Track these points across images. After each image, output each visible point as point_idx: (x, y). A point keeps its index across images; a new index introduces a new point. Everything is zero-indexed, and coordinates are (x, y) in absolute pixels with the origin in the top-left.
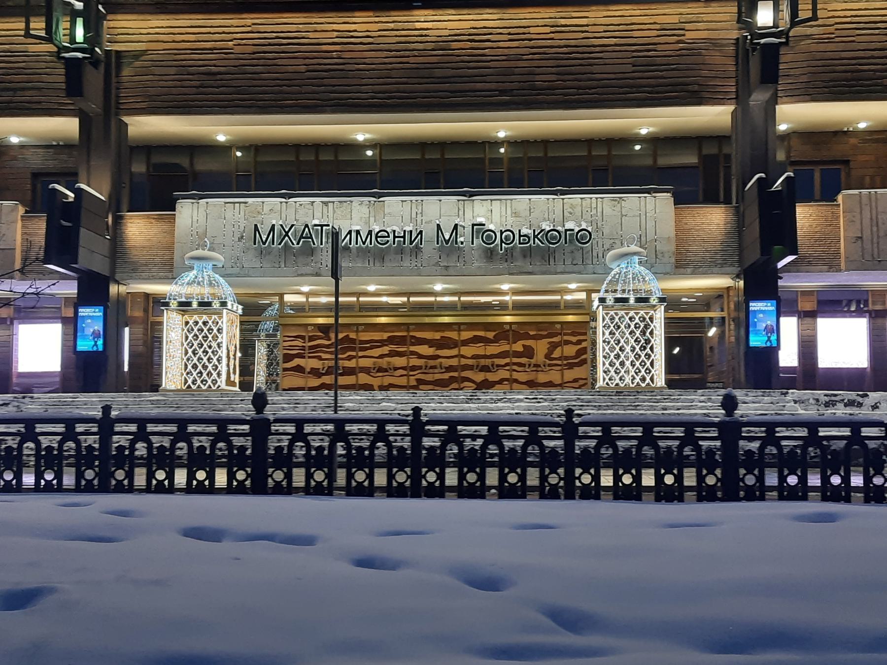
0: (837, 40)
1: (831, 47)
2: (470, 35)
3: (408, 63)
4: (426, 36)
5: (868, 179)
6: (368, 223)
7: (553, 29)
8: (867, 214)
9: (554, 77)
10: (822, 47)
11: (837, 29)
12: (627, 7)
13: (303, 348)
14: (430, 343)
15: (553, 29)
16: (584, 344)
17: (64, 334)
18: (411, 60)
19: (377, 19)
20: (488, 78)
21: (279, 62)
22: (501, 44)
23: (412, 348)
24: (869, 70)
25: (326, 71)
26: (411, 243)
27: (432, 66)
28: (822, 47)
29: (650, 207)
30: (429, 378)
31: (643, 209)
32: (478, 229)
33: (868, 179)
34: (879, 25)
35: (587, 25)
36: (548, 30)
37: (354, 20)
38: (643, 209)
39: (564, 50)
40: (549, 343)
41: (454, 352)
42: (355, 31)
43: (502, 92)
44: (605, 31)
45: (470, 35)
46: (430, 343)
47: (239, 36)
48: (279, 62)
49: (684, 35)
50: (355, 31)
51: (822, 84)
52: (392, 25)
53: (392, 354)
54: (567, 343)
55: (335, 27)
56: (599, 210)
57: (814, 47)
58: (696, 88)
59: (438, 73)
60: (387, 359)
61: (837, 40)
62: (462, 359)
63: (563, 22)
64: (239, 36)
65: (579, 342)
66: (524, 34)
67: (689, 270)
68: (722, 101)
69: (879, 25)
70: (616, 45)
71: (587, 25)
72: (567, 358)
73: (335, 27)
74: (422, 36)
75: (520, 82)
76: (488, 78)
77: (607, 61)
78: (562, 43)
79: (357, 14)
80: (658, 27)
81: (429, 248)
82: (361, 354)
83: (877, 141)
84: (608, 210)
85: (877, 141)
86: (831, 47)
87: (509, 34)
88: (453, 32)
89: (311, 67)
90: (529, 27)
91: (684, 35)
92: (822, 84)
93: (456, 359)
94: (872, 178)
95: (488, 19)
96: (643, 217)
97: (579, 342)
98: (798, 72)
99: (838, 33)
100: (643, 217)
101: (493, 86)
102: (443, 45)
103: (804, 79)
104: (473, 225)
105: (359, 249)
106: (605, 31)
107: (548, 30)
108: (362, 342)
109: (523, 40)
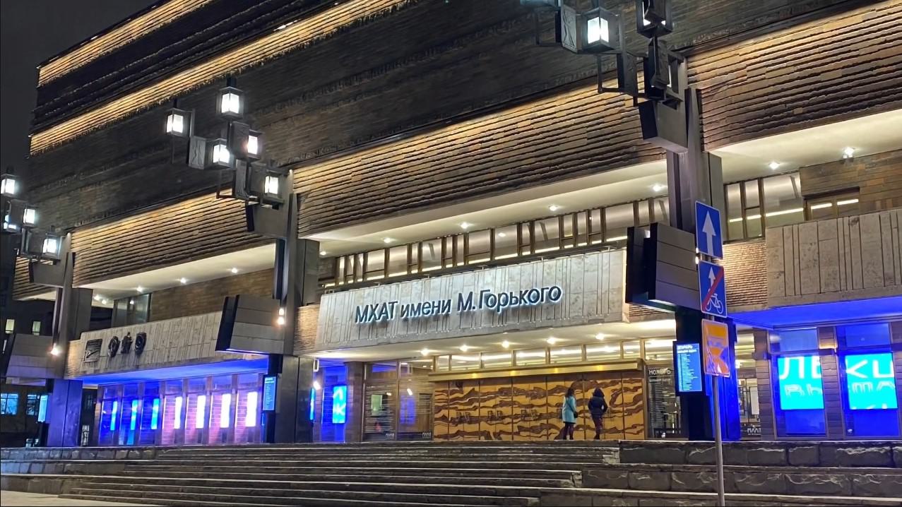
0: (749, 80)
1: (745, 88)
2: (480, 138)
3: (444, 168)
4: (454, 145)
5: (878, 204)
6: (420, 298)
7: (533, 121)
8: (788, 246)
9: (533, 160)
10: (736, 90)
11: (748, 71)
12: (582, 91)
13: (447, 401)
14: (526, 393)
15: (533, 121)
16: (640, 391)
17: (258, 396)
18: (445, 165)
19: (426, 139)
20: (492, 170)
21: (375, 183)
22: (500, 141)
23: (515, 399)
24: (781, 103)
25: (398, 184)
26: (443, 311)
27: (460, 166)
28: (736, 90)
29: (605, 261)
30: (526, 425)
31: (600, 264)
32: (486, 297)
33: (878, 204)
34: (786, 58)
35: (555, 113)
36: (530, 122)
37: (416, 142)
38: (600, 264)
39: (541, 136)
40: (613, 390)
41: (543, 401)
42: (415, 151)
43: (501, 178)
44: (567, 115)
45: (480, 138)
46: (526, 393)
47: (354, 169)
48: (375, 183)
49: (624, 105)
50: (415, 151)
51: (738, 125)
52: (435, 142)
53: (502, 404)
54: (627, 390)
55: (404, 150)
56: (569, 268)
57: (729, 92)
58: (634, 149)
59: (462, 171)
60: (499, 409)
61: (749, 80)
62: (549, 408)
63: (539, 114)
64: (354, 169)
65: (636, 389)
66: (514, 129)
67: (642, 317)
68: (658, 157)
69: (786, 58)
70: (575, 124)
71: (555, 113)
72: (627, 405)
73: (404, 150)
74: (452, 145)
75: (500, 171)
76: (492, 170)
77: (570, 139)
78: (538, 131)
79: (415, 138)
80: (605, 102)
81: (454, 312)
82: (482, 404)
83: (885, 163)
84: (575, 267)
85: (885, 163)
86: (745, 88)
87: (505, 131)
88: (470, 138)
89: (391, 183)
90: (517, 123)
91: (624, 105)
92: (738, 125)
93: (545, 408)
94: (883, 201)
95: (491, 123)
96: (600, 271)
97: (636, 389)
98: (718, 118)
99: (749, 74)
100: (600, 271)
101: (495, 175)
102: (464, 150)
103: (723, 123)
104: (482, 292)
105: (414, 319)
106: (567, 115)
107: (530, 122)
108: (484, 394)
109: (513, 134)
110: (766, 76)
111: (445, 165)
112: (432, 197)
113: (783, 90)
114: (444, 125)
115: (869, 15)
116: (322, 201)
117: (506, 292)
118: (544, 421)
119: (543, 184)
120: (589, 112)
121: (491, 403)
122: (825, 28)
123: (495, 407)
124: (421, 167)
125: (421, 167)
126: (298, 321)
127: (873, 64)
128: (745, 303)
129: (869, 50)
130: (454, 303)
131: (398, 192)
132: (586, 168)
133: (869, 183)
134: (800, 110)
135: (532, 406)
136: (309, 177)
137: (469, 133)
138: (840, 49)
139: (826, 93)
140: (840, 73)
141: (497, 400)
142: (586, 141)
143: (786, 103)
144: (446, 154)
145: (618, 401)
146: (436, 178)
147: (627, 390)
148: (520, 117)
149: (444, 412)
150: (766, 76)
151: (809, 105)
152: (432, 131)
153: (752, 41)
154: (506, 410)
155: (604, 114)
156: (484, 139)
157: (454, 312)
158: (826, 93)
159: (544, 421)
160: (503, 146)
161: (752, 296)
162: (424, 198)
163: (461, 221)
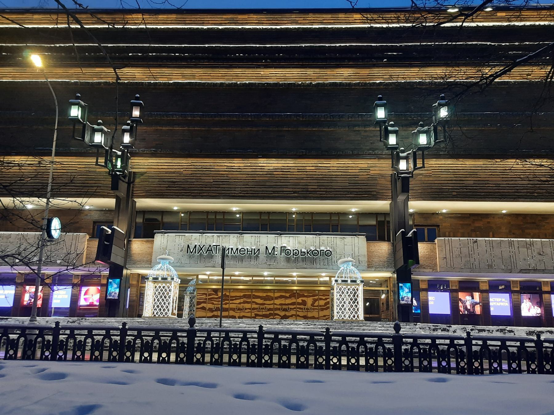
5: (447, 233)
10: (427, 179)
16: (328, 300)
18: (257, 178)
20: (289, 187)
22: (294, 173)
28: (427, 179)
41: (272, 302)
43: (295, 192)
48: (202, 178)
53: (245, 302)
54: (321, 299)
55: (226, 164)
57: (423, 179)
63: (320, 165)
65: (326, 299)
67: (373, 269)
72: (320, 306)
76: (289, 187)
81: (262, 256)
94: (449, 232)
97: (326, 299)
101: (291, 190)
110: (441, 176)
111: (257, 178)
112: (247, 194)
113: (448, 183)
114: (257, 157)
115: (485, 163)
116: (157, 180)
117: (318, 249)
118: (272, 312)
119: (321, 200)
120: (350, 171)
121: (238, 301)
122: (467, 163)
123: (240, 303)
124: (238, 176)
125: (238, 176)
126: (130, 248)
127: (486, 182)
128: (424, 268)
129: (485, 176)
130: (263, 250)
131: (221, 186)
132: (348, 197)
133: (444, 224)
134: (455, 193)
135: (265, 304)
136: (142, 164)
137: (273, 165)
138: (473, 173)
139: (467, 189)
140: (472, 182)
141: (242, 300)
142: (348, 184)
143: (449, 189)
144: (257, 173)
145: (316, 304)
146: (249, 183)
147: (321, 299)
148: (309, 164)
149: (202, 305)
150: (441, 176)
151: (459, 192)
152: (252, 158)
153: (435, 160)
154: (248, 306)
155: (358, 174)
156: (284, 170)
157: (262, 256)
158: (467, 189)
159: (272, 312)
160: (296, 176)
161: (427, 266)
162: (240, 193)
163: (233, 207)
